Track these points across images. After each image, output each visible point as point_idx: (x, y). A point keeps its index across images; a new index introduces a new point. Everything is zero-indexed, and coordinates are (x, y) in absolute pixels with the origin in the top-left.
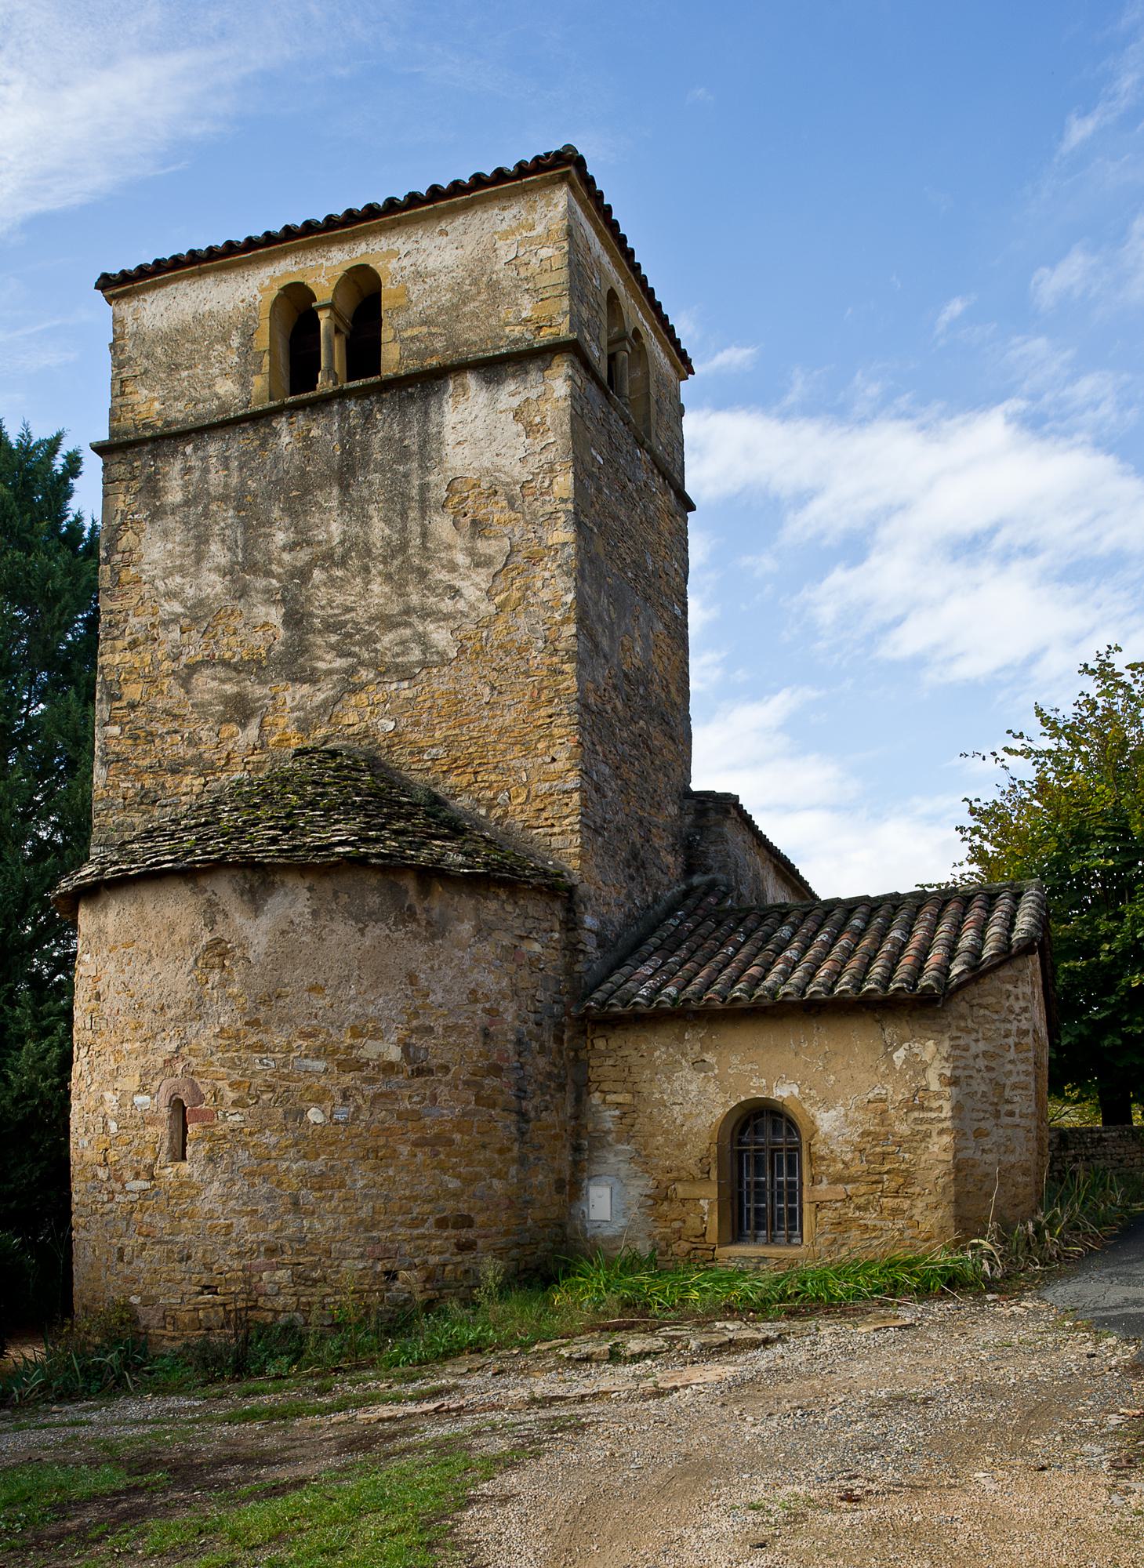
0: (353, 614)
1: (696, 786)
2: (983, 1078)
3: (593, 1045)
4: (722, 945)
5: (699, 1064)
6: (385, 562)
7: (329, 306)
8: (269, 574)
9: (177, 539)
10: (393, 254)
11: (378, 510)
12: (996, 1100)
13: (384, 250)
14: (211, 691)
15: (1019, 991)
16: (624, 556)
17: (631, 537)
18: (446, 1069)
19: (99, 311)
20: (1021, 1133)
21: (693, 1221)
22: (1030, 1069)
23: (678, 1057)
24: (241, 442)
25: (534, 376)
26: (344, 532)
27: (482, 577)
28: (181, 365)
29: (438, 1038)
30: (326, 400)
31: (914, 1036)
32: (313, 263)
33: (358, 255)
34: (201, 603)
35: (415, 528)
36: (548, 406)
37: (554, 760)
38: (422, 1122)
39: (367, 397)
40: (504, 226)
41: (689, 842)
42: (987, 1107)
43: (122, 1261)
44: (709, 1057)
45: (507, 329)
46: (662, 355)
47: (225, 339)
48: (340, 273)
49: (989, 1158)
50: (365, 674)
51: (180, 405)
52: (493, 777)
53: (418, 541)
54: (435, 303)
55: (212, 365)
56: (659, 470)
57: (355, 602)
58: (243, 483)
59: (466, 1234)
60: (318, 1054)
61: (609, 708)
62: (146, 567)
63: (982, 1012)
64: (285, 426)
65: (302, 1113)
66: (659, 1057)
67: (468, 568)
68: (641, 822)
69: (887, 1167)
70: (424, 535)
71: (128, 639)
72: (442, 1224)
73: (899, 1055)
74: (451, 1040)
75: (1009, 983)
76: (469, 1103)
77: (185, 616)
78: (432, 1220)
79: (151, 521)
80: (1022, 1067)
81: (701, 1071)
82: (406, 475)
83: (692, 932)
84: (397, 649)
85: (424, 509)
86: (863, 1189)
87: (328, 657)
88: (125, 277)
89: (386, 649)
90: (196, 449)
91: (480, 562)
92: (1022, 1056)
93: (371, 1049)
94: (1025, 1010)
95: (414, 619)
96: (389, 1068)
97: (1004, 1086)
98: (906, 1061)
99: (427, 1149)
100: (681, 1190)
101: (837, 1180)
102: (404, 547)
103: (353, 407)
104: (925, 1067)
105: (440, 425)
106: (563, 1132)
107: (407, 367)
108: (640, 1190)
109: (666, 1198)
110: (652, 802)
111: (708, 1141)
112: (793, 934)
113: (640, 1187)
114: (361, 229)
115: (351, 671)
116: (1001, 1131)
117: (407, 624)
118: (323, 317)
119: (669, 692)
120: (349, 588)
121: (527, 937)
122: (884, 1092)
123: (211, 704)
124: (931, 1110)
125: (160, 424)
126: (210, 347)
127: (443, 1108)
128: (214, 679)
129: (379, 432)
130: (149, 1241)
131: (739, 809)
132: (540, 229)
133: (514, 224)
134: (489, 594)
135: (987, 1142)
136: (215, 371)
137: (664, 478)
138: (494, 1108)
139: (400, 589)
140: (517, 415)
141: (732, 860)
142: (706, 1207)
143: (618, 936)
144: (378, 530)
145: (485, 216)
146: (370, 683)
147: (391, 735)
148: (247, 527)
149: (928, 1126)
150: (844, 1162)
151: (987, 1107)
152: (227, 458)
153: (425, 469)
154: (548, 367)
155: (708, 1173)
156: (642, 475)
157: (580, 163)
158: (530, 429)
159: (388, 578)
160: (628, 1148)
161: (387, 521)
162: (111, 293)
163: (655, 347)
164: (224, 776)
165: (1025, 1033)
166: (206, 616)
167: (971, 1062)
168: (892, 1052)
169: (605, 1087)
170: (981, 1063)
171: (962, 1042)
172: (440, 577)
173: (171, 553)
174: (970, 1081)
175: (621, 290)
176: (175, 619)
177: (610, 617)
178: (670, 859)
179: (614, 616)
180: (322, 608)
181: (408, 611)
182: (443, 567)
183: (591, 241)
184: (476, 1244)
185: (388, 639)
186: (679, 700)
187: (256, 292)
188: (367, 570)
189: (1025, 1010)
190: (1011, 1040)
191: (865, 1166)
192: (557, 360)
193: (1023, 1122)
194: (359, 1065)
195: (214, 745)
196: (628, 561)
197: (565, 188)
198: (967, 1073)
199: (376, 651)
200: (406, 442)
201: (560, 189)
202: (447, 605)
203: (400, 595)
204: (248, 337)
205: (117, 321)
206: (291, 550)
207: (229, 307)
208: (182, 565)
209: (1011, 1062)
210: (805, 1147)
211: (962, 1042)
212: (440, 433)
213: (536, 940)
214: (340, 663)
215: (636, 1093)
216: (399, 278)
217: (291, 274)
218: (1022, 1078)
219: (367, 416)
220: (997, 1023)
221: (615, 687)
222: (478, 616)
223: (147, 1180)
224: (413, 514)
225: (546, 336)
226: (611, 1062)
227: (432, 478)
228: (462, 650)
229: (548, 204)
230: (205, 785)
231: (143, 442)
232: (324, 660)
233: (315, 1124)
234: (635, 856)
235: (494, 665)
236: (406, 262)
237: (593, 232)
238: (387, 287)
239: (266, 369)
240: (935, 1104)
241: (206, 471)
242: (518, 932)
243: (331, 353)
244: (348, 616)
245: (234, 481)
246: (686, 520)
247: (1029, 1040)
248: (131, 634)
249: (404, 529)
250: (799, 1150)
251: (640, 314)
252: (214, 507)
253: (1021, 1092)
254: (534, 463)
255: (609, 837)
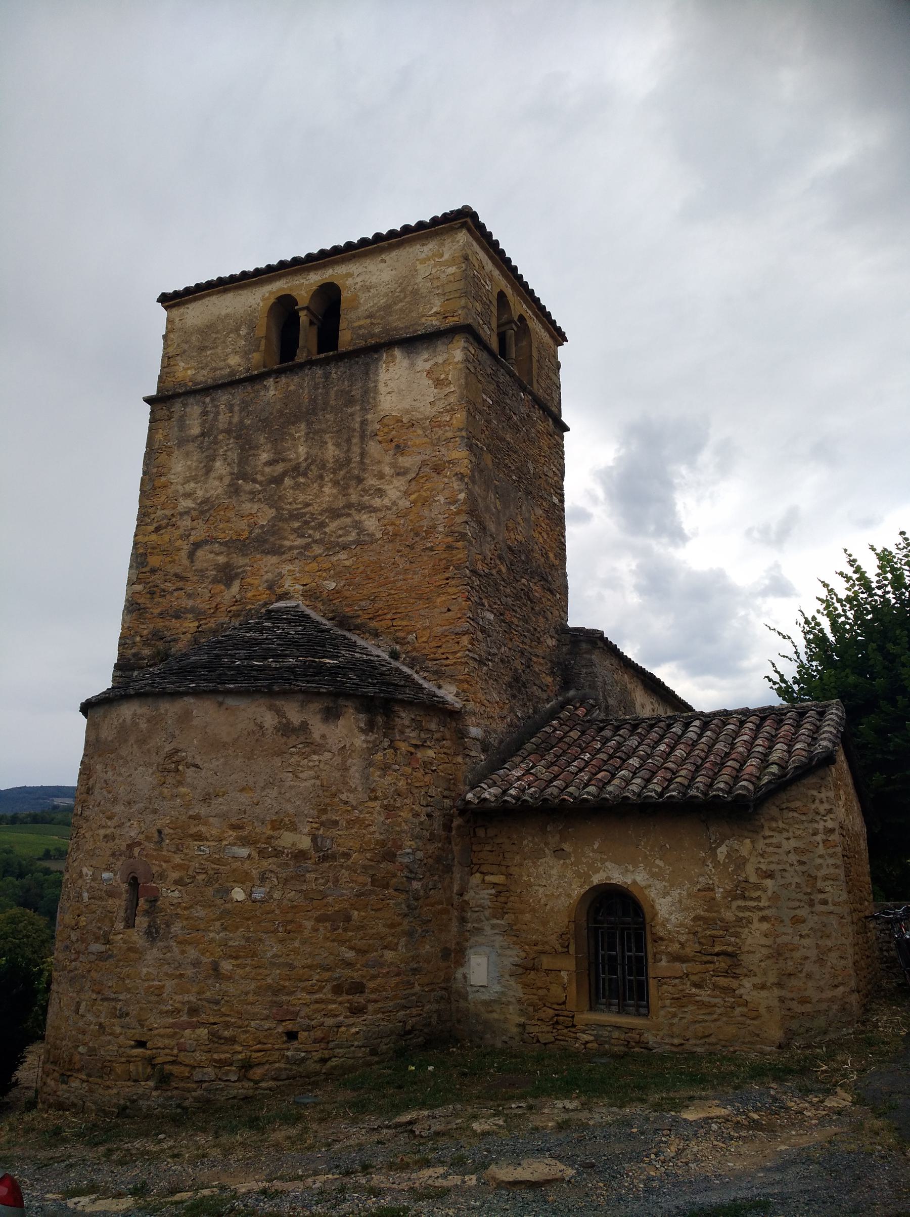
0: (311, 508)
1: (572, 623)
2: (796, 871)
3: (475, 832)
4: (583, 751)
5: (559, 852)
6: (334, 473)
7: (307, 308)
8: (254, 481)
9: (195, 458)
10: (350, 275)
11: (332, 438)
12: (809, 890)
13: (344, 273)
14: (206, 561)
15: (823, 795)
16: (510, 465)
17: (515, 452)
18: (347, 855)
19: (161, 314)
20: (833, 921)
21: (556, 990)
22: (839, 862)
23: (542, 845)
24: (238, 396)
25: (441, 347)
26: (308, 453)
27: (400, 483)
28: (207, 347)
29: (342, 830)
30: (301, 366)
31: (734, 835)
32: (297, 282)
33: (327, 276)
34: (206, 501)
35: (356, 450)
36: (451, 367)
37: (449, 610)
38: (325, 901)
39: (328, 364)
40: (423, 256)
41: (566, 666)
42: (801, 896)
43: (78, 1013)
44: (567, 847)
45: (423, 320)
46: (543, 331)
47: (237, 330)
48: (315, 288)
49: (806, 942)
50: (317, 550)
51: (205, 372)
52: (404, 623)
53: (358, 459)
54: (376, 304)
55: (227, 346)
56: (539, 405)
57: (312, 499)
58: (241, 422)
59: (359, 999)
60: (245, 841)
61: (494, 572)
62: (173, 477)
63: (791, 814)
64: (272, 383)
65: (228, 891)
66: (527, 845)
67: (392, 476)
68: (523, 653)
69: (717, 949)
70: (363, 455)
71: (155, 525)
72: (337, 990)
73: (722, 851)
74: (353, 831)
75: (813, 789)
76: (366, 884)
77: (194, 509)
78: (329, 987)
79: (179, 447)
80: (831, 861)
81: (560, 859)
82: (352, 415)
83: (560, 739)
84: (340, 532)
85: (363, 437)
86: (699, 967)
87: (292, 537)
88: (176, 294)
89: (332, 532)
90: (212, 400)
91: (401, 472)
92: (831, 851)
93: (287, 839)
94: (830, 811)
95: (353, 512)
96: (301, 855)
97: (816, 878)
98: (728, 856)
99: (328, 924)
100: (546, 962)
101: (676, 958)
102: (349, 461)
103: (319, 372)
104: (745, 861)
105: (376, 381)
106: (450, 907)
107: (355, 344)
108: (511, 959)
109: (533, 969)
110: (532, 637)
111: (567, 920)
112: (640, 744)
113: (514, 956)
114: (329, 261)
115: (307, 547)
116: (816, 918)
117: (349, 515)
118: (303, 315)
119: (548, 558)
120: (309, 490)
121: (422, 745)
122: (711, 882)
123: (207, 570)
124: (752, 899)
125: (190, 384)
126: (227, 335)
127: (343, 889)
128: (211, 553)
129: (335, 386)
130: (100, 997)
131: (605, 641)
132: (446, 256)
133: (430, 254)
134: (406, 494)
135: (804, 929)
136: (229, 350)
137: (544, 411)
138: (387, 889)
139: (344, 490)
140: (429, 373)
141: (601, 679)
142: (566, 978)
143: (501, 742)
144: (331, 451)
145: (411, 250)
146: (320, 555)
147: (333, 592)
148: (242, 448)
149: (750, 914)
150: (680, 943)
151: (801, 896)
152: (232, 405)
153: (364, 410)
154: (451, 342)
155: (568, 947)
156: (523, 410)
157: (474, 216)
158: (438, 383)
159: (336, 483)
160: (502, 922)
161: (337, 445)
162: (167, 304)
163: (535, 325)
164: (212, 620)
165: (832, 831)
166: (209, 510)
167: (785, 858)
168: (716, 848)
169: (484, 869)
170: (793, 858)
171: (774, 840)
172: (372, 482)
173: (190, 468)
174: (785, 874)
175: (509, 291)
176: (187, 512)
177: (496, 507)
178: (549, 679)
179: (499, 507)
180: (290, 504)
181: (349, 506)
182: (375, 476)
183: (484, 263)
184: (366, 1008)
185: (333, 526)
186: (557, 562)
187: (259, 301)
188: (321, 477)
189: (830, 811)
190: (819, 838)
191: (697, 947)
192: (457, 337)
193: (837, 909)
194: (277, 853)
195: (207, 599)
196: (513, 468)
197: (464, 231)
198: (780, 867)
199: (325, 533)
200: (353, 393)
201: (461, 232)
202: (377, 502)
203: (344, 495)
204: (252, 328)
205: (169, 321)
206: (271, 464)
207: (242, 311)
208: (196, 475)
209: (820, 856)
210: (648, 927)
211: (774, 840)
212: (376, 386)
213: (429, 747)
214: (299, 542)
215: (509, 875)
216: (352, 289)
217: (282, 289)
218: (832, 870)
219: (327, 376)
220: (806, 824)
221: (500, 558)
222: (397, 510)
223: (104, 944)
224: (355, 440)
225: (451, 322)
226: (488, 848)
227: (369, 417)
228: (385, 533)
229: (453, 242)
230: (198, 627)
231: (179, 395)
232: (289, 540)
233: (237, 901)
234: (517, 679)
235: (407, 543)
236: (358, 280)
237: (486, 257)
238: (345, 295)
239: (262, 348)
240: (755, 894)
241: (217, 413)
242: (414, 742)
243: (308, 337)
244: (307, 510)
245: (236, 420)
246: (562, 438)
247: (835, 837)
248: (158, 521)
249: (349, 450)
250: (644, 929)
251: (524, 306)
252: (220, 437)
253: (831, 882)
254: (440, 405)
255: (493, 666)
